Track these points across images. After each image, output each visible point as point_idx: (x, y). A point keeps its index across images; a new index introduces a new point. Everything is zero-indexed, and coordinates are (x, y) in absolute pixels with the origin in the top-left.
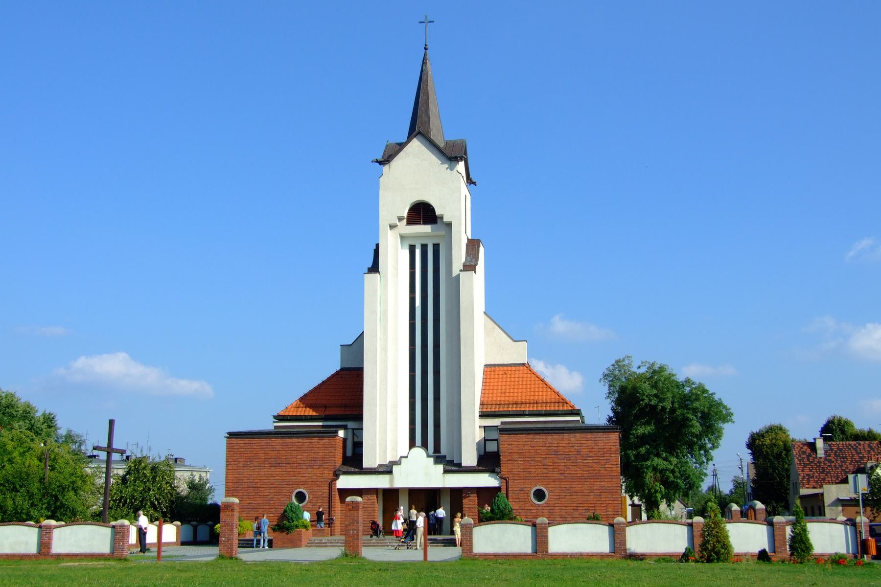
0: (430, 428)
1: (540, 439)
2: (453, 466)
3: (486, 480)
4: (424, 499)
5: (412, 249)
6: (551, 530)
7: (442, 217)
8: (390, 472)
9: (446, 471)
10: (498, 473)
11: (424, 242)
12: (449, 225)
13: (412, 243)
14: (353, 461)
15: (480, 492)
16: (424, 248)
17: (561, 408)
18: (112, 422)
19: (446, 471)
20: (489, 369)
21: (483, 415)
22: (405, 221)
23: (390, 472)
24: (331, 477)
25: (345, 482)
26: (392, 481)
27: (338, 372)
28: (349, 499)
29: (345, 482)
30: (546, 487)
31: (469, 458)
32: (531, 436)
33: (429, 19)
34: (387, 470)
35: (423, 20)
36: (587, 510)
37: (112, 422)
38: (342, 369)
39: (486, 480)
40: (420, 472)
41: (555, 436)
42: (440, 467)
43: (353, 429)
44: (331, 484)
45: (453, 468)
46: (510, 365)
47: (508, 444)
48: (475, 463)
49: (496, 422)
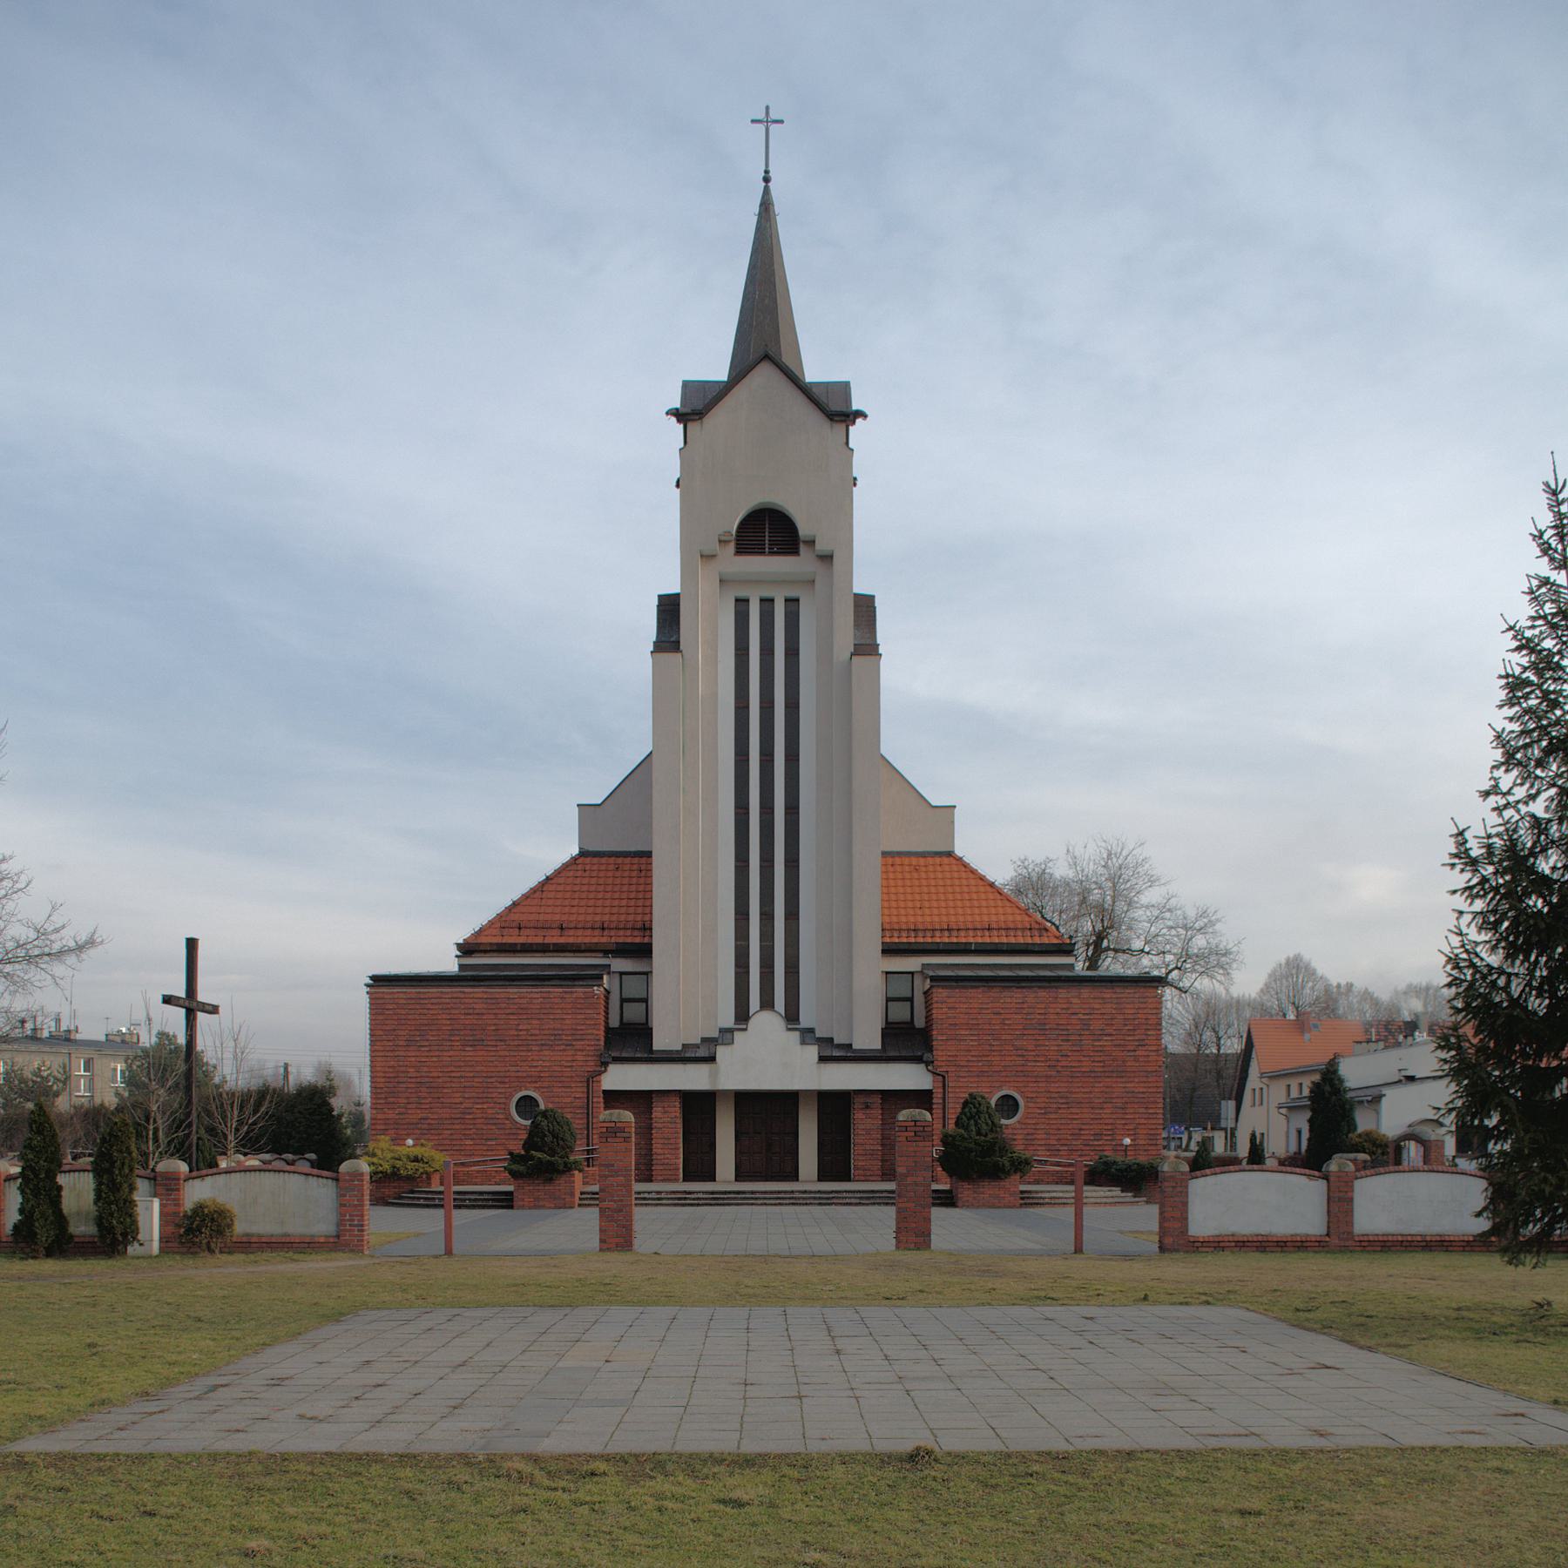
0: (768, 975)
1: (1012, 997)
2: (835, 1052)
3: (906, 1077)
4: (767, 1112)
5: (742, 603)
6: (1357, 1183)
7: (811, 543)
8: (711, 1059)
9: (823, 1059)
10: (927, 1063)
11: (767, 594)
12: (827, 558)
13: (742, 594)
14: (632, 1039)
15: (893, 1099)
16: (767, 602)
17: (1037, 940)
18: (192, 944)
19: (823, 1059)
20: (890, 861)
21: (889, 950)
22: (732, 547)
23: (711, 1059)
24: (592, 1066)
25: (620, 1077)
26: (714, 1076)
27: (574, 860)
28: (904, 1115)
29: (620, 1077)
30: (1017, 1089)
31: (868, 1036)
32: (995, 993)
33: (773, 116)
34: (702, 1053)
35: (762, 116)
36: (1098, 1136)
37: (192, 944)
38: (583, 853)
39: (906, 1077)
40: (768, 1059)
41: (1042, 993)
42: (812, 1052)
43: (621, 974)
44: (593, 1077)
45: (836, 1053)
46: (924, 855)
47: (951, 1007)
48: (876, 1044)
49: (912, 963)
